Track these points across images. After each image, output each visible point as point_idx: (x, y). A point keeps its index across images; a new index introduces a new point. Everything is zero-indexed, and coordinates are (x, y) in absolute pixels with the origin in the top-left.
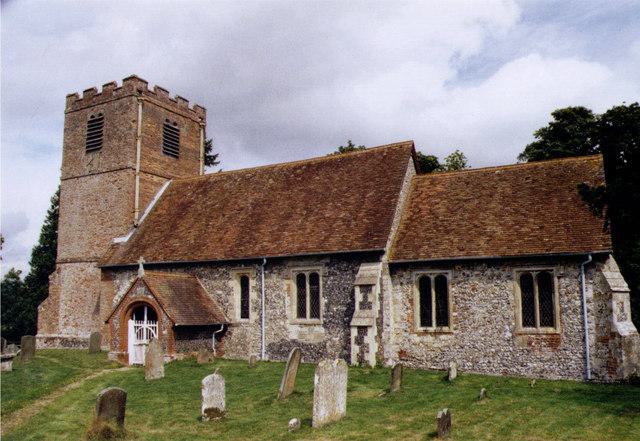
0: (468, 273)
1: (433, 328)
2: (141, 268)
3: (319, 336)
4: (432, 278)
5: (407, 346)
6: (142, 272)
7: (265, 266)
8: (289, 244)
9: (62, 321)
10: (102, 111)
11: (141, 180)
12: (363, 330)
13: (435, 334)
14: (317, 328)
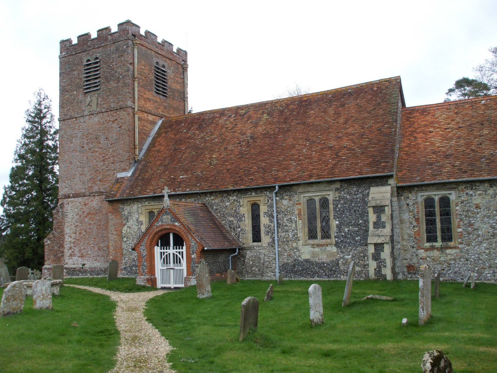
0: (471, 192)
1: (439, 244)
2: (166, 198)
3: (332, 254)
4: (437, 199)
5: (415, 260)
6: (167, 201)
7: (276, 193)
9: (67, 252)
10: (98, 55)
11: (139, 119)
12: (379, 247)
13: (442, 249)
14: (329, 248)
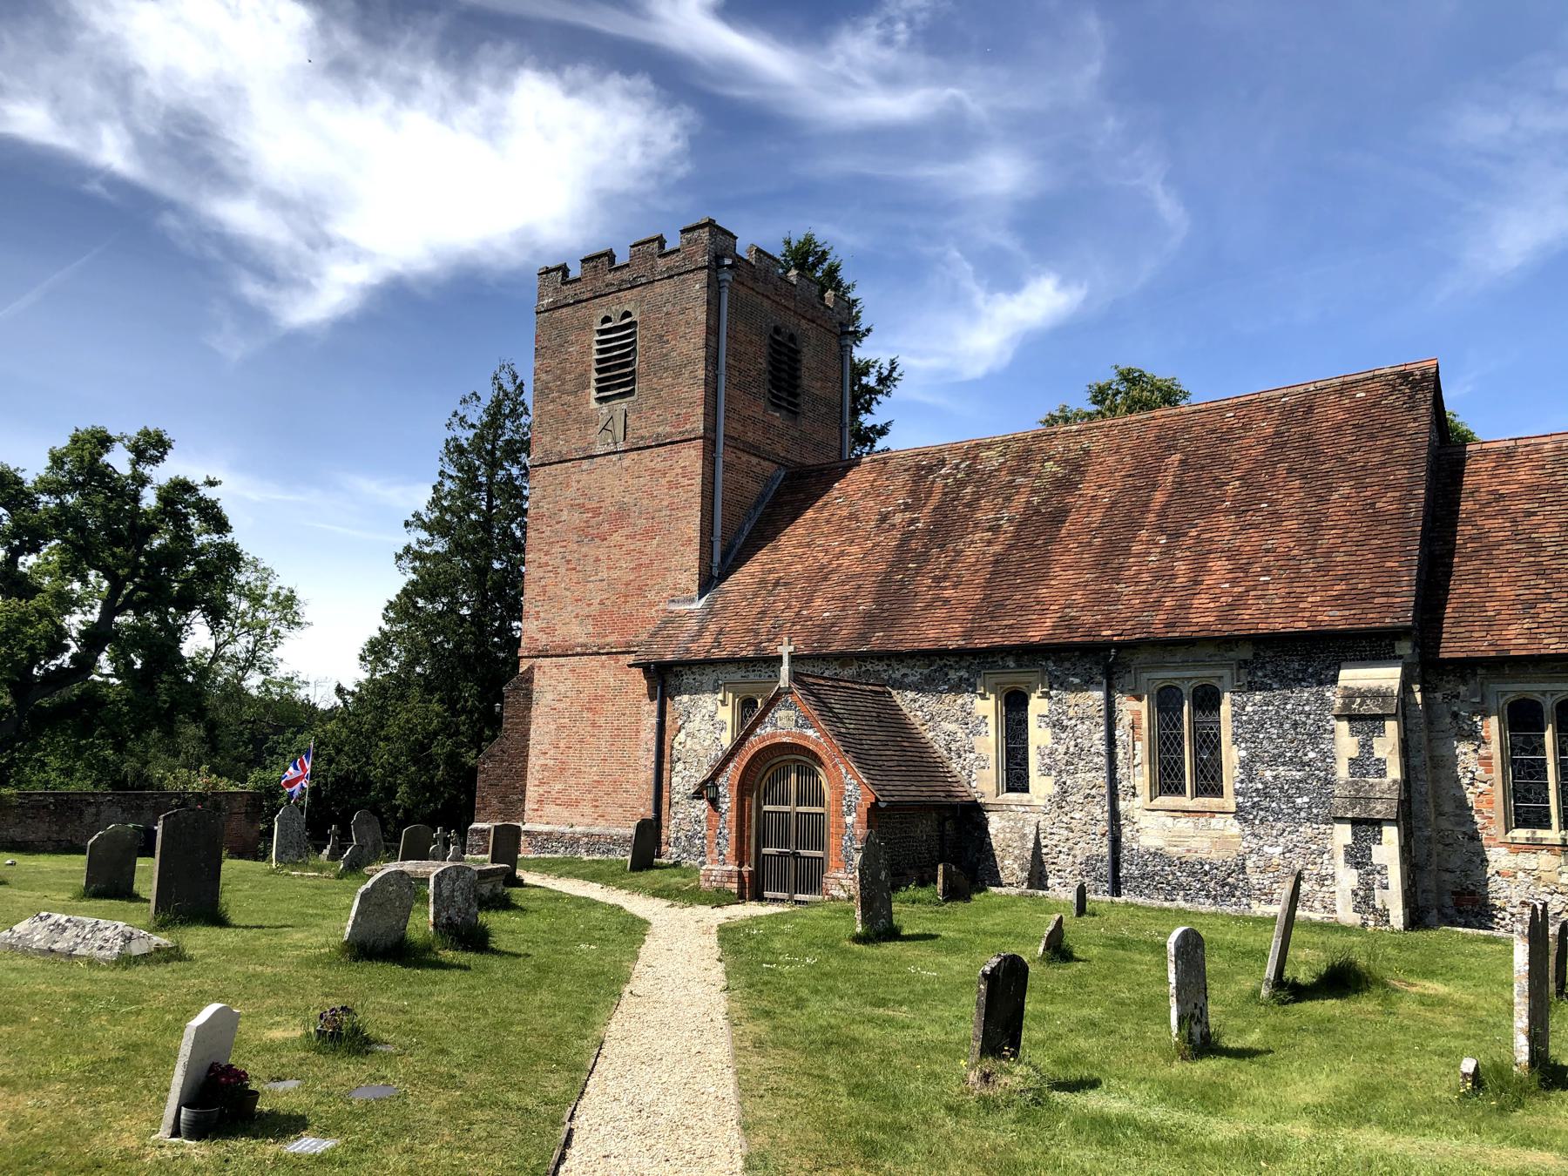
8: (1130, 611)
14: (1217, 822)
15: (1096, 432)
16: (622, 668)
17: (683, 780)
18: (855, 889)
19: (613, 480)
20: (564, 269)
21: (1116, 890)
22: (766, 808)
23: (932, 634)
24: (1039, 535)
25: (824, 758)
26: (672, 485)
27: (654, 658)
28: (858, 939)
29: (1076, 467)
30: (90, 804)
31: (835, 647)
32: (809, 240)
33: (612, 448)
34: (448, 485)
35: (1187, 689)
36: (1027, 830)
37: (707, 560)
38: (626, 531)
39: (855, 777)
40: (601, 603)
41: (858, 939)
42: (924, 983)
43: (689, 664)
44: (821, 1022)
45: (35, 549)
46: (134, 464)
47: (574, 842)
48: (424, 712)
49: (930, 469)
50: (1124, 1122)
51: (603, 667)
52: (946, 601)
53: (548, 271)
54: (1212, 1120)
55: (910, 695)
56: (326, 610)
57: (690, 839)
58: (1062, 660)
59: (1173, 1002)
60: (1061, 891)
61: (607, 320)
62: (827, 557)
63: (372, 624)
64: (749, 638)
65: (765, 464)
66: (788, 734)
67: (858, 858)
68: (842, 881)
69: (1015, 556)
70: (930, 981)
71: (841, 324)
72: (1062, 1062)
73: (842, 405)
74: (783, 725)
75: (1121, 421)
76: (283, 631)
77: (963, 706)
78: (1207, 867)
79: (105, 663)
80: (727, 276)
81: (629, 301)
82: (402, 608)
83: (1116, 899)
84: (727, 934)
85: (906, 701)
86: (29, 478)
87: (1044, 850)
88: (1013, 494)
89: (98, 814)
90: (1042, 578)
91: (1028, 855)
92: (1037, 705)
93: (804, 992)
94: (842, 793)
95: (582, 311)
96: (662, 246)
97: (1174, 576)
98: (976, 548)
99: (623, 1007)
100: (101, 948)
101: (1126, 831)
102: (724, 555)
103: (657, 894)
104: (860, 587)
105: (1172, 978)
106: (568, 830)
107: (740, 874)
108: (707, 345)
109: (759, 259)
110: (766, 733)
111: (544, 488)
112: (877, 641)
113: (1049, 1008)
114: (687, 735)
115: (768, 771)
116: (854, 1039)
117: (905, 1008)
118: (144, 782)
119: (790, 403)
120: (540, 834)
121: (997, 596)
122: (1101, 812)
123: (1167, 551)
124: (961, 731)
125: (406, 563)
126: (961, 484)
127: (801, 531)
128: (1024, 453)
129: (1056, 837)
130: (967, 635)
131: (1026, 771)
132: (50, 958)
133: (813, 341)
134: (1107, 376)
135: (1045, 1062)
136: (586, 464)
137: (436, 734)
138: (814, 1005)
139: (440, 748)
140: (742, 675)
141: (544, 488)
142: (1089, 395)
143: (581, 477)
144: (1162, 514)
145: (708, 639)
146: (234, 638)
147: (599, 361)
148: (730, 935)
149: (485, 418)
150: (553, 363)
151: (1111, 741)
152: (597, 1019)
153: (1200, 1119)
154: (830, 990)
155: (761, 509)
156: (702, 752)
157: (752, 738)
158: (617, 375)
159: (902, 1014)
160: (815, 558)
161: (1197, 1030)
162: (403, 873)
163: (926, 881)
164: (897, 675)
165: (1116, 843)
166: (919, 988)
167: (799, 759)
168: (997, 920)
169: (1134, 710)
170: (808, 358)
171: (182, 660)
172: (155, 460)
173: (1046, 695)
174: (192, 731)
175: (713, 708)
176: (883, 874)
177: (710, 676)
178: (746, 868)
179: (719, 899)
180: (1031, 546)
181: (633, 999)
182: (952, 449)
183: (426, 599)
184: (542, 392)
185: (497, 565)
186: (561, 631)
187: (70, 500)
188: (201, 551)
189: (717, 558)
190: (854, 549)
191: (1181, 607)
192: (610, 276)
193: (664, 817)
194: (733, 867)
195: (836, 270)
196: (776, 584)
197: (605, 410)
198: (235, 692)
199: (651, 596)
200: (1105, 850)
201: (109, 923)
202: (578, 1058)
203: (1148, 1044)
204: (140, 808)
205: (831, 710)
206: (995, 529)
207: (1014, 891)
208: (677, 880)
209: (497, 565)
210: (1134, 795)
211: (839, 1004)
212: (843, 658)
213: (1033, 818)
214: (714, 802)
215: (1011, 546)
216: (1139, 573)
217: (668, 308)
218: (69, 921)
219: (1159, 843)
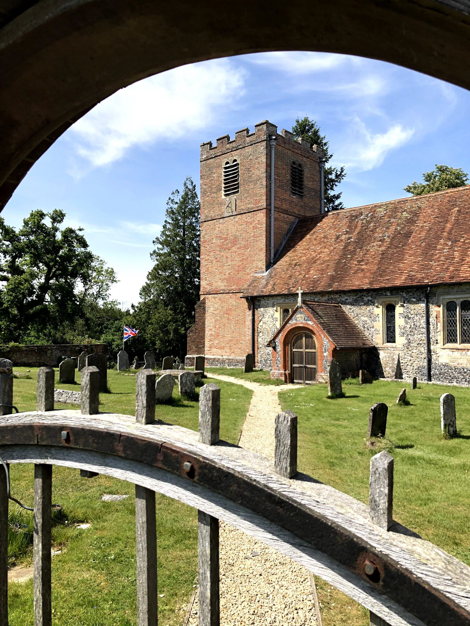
8: (436, 273)
15: (423, 199)
16: (238, 298)
17: (263, 339)
18: (328, 380)
19: (231, 226)
20: (210, 144)
21: (430, 379)
22: (294, 350)
23: (357, 283)
24: (400, 242)
25: (315, 331)
26: (255, 228)
27: (250, 295)
28: (329, 397)
29: (415, 214)
30: (49, 349)
31: (319, 289)
32: (306, 120)
33: (231, 214)
34: (168, 226)
35: (458, 302)
36: (395, 357)
37: (269, 256)
38: (238, 246)
39: (327, 339)
40: (229, 274)
41: (329, 397)
42: (353, 413)
43: (263, 297)
44: (316, 425)
45: (21, 256)
46: (53, 223)
47: (223, 362)
48: (164, 313)
49: (356, 217)
50: (419, 458)
51: (231, 298)
52: (363, 270)
53: (204, 145)
54: (452, 458)
55: (348, 307)
56: (125, 277)
57: (266, 361)
58: (409, 292)
59: (442, 420)
60: (407, 380)
61: (227, 163)
62: (316, 252)
63: (143, 281)
64: (286, 286)
65: (290, 217)
66: (302, 323)
67: (329, 368)
68: (323, 376)
69: (390, 251)
70: (355, 412)
71: (320, 158)
72: (402, 440)
73: (320, 191)
74: (300, 319)
75: (434, 195)
76: (110, 284)
77: (369, 310)
78: (465, 370)
79: (47, 297)
80: (274, 143)
81: (236, 155)
82: (154, 275)
83: (429, 382)
84: (281, 395)
85: (346, 309)
86: (17, 231)
87: (401, 364)
88: (390, 227)
89: (52, 353)
90: (401, 260)
91: (395, 366)
92: (399, 310)
93: (310, 416)
94: (322, 345)
95: (217, 160)
96: (248, 132)
97: (454, 258)
98: (375, 248)
99: (247, 420)
100: (75, 400)
101: (434, 357)
102: (275, 255)
103: (255, 381)
104: (328, 265)
105: (442, 411)
106: (221, 357)
107: (285, 374)
108: (266, 172)
109: (286, 135)
110: (293, 323)
111: (206, 231)
112: (336, 286)
113: (399, 422)
114: (263, 323)
115: (295, 337)
116: (328, 431)
117: (346, 421)
118: (64, 341)
119: (300, 192)
120: (211, 359)
121: (383, 268)
122: (424, 350)
123: (451, 248)
124: (368, 320)
125: (154, 257)
126: (369, 222)
127: (305, 243)
128: (395, 208)
129: (406, 360)
130: (371, 283)
131: (394, 335)
132: (59, 403)
133: (309, 166)
134: (432, 169)
135: (393, 438)
136: (221, 221)
137: (170, 321)
138: (313, 420)
139: (171, 327)
140: (284, 300)
141: (206, 231)
142: (424, 178)
143: (220, 226)
144: (450, 233)
145: (270, 287)
146: (91, 287)
147: (225, 180)
148: (282, 396)
149: (181, 200)
150: (208, 181)
151: (428, 323)
152: (239, 424)
153: (447, 458)
154: (319, 415)
155: (289, 235)
156: (269, 329)
157: (288, 325)
158: (232, 184)
159: (345, 423)
160: (311, 254)
161: (451, 429)
162: (170, 375)
163: (355, 376)
164: (344, 299)
165: (429, 361)
166: (351, 414)
167: (306, 332)
168: (382, 391)
169: (437, 311)
170: (307, 173)
171: (75, 296)
172: (60, 222)
173: (402, 306)
174: (81, 322)
175: (272, 313)
176: (338, 375)
177: (271, 301)
178: (287, 372)
179: (278, 383)
180: (397, 247)
181: (250, 417)
182: (365, 208)
183: (162, 271)
184: (204, 193)
185: (188, 257)
186: (215, 285)
187: (32, 238)
188: (78, 255)
189: (272, 256)
190: (326, 250)
191: (456, 270)
192: (228, 146)
193: (256, 353)
194: (282, 371)
195: (317, 131)
196: (295, 265)
197: (228, 199)
198: (94, 307)
199: (248, 271)
200: (426, 364)
201: (76, 392)
202: (234, 436)
203: (434, 434)
204: (66, 351)
205: (317, 314)
206: (382, 240)
207: (389, 380)
208: (261, 376)
209: (188, 257)
210: (437, 343)
211: (322, 419)
212: (322, 293)
213: (397, 352)
214: (274, 348)
215: (388, 247)
216: (440, 257)
217: (251, 157)
218: (63, 391)
219: (447, 361)
